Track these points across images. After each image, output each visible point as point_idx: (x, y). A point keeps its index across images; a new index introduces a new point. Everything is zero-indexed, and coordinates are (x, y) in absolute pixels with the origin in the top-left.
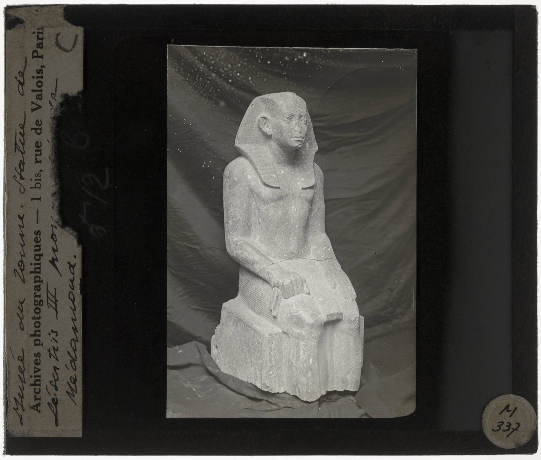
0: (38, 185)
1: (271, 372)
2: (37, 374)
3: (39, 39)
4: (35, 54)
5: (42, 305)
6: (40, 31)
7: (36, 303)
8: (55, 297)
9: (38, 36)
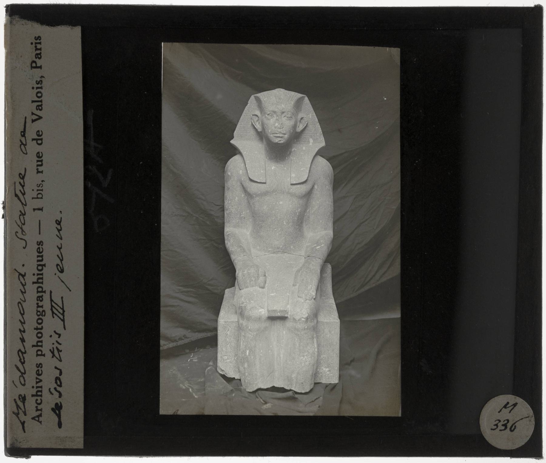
0: (40, 196)
1: (226, 357)
2: (38, 385)
3: (37, 49)
4: (34, 65)
5: (44, 315)
6: (38, 41)
7: (39, 313)
8: (63, 309)
9: (36, 47)
